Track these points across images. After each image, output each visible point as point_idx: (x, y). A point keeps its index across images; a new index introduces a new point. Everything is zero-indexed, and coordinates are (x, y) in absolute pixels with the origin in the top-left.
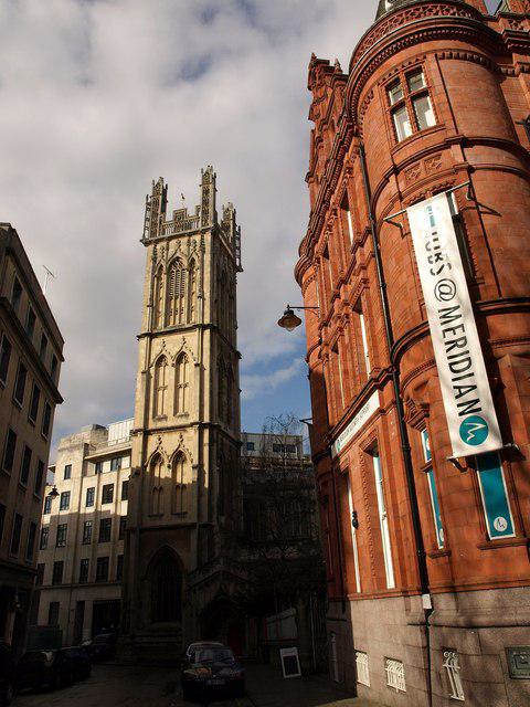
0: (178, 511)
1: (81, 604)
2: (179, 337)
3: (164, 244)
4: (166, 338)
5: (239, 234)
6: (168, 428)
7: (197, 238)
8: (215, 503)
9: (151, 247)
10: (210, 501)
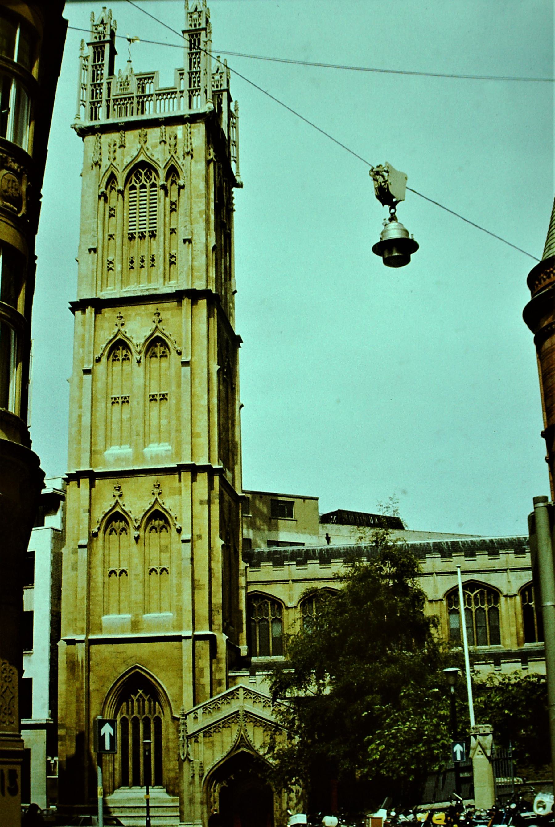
3: (115, 136)
7: (180, 130)
9: (91, 139)
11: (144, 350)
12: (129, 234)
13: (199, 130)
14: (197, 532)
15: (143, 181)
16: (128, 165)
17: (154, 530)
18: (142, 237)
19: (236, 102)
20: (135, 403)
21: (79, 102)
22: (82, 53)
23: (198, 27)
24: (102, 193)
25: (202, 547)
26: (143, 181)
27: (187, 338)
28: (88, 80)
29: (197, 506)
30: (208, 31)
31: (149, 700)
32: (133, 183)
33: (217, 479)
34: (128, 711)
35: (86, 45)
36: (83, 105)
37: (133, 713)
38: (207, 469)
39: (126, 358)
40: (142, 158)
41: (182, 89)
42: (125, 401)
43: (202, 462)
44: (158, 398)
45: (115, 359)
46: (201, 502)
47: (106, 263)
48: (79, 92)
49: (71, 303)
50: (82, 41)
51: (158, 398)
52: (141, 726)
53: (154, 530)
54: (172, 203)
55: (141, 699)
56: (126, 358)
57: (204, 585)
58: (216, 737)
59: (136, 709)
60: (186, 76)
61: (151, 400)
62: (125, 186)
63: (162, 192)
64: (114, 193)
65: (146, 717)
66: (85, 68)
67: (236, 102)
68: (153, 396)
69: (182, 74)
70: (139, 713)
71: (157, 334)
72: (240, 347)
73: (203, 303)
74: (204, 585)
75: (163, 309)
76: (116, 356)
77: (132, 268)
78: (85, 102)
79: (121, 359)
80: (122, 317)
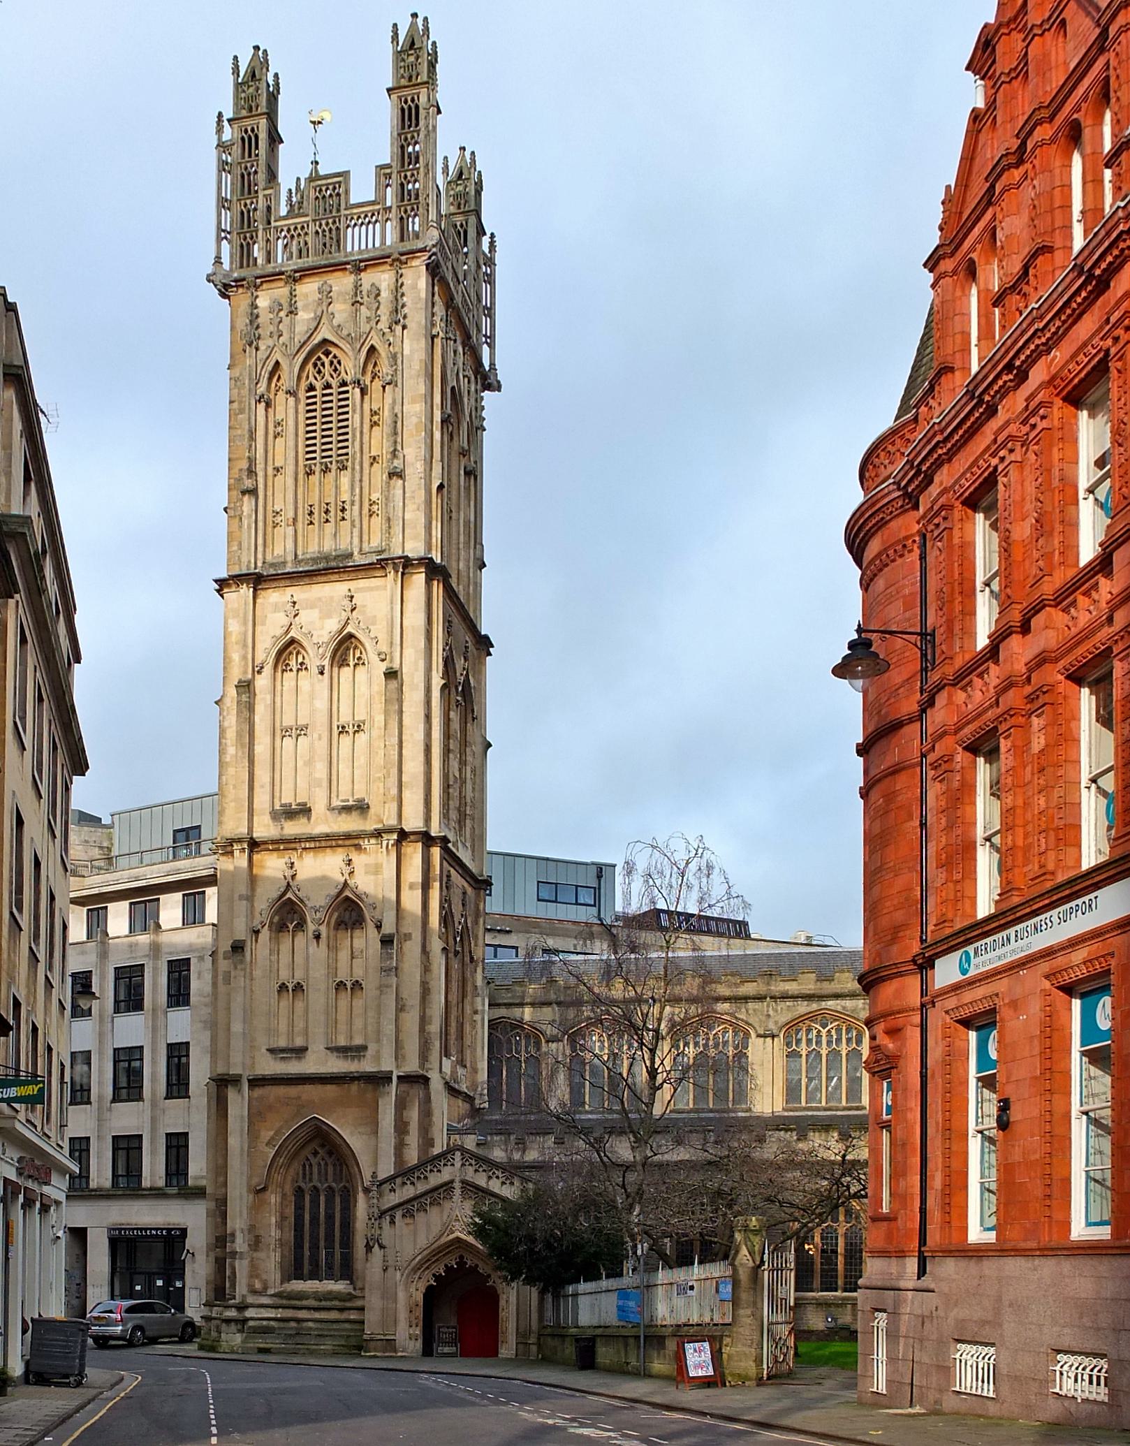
0: (342, 1042)
1: (79, 1235)
2: (335, 590)
3: (280, 291)
4: (301, 593)
5: (490, 262)
6: (311, 839)
7: (383, 278)
8: (435, 1027)
9: (242, 298)
10: (424, 1021)
11: (328, 655)
12: (305, 466)
13: (417, 279)
14: (404, 930)
15: (327, 377)
16: (301, 347)
17: (343, 926)
18: (326, 470)
19: (492, 236)
20: (316, 736)
21: (218, 235)
22: (219, 139)
23: (414, 81)
24: (262, 396)
25: (412, 949)
26: (327, 377)
27: (249, 549)
28: (232, 192)
29: (404, 887)
30: (431, 87)
31: (334, 1165)
32: (311, 379)
33: (436, 852)
34: (304, 1177)
35: (226, 123)
36: (226, 238)
37: (311, 1180)
38: (427, 839)
39: (302, 666)
40: (325, 333)
41: (388, 204)
42: (302, 730)
43: (413, 822)
44: (351, 731)
45: (343, 663)
46: (411, 887)
47: (270, 515)
48: (219, 215)
49: (216, 581)
50: (220, 115)
51: (351, 731)
52: (322, 1198)
53: (343, 926)
54: (374, 413)
55: (322, 1163)
56: (302, 666)
57: (225, 958)
58: (420, 1217)
59: (315, 1176)
60: (394, 180)
61: (340, 732)
62: (298, 385)
63: (357, 391)
64: (281, 396)
65: (315, 1187)
66: (223, 166)
67: (492, 236)
68: (343, 727)
69: (389, 176)
70: (334, 1181)
71: (349, 629)
72: (490, 654)
73: (419, 579)
74: (225, 958)
75: (359, 590)
76: (288, 665)
77: (311, 523)
78: (229, 233)
79: (294, 669)
80: (294, 603)
